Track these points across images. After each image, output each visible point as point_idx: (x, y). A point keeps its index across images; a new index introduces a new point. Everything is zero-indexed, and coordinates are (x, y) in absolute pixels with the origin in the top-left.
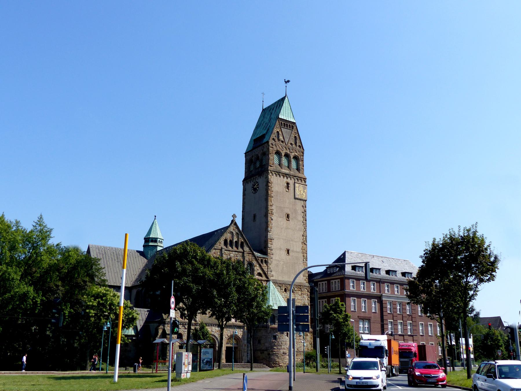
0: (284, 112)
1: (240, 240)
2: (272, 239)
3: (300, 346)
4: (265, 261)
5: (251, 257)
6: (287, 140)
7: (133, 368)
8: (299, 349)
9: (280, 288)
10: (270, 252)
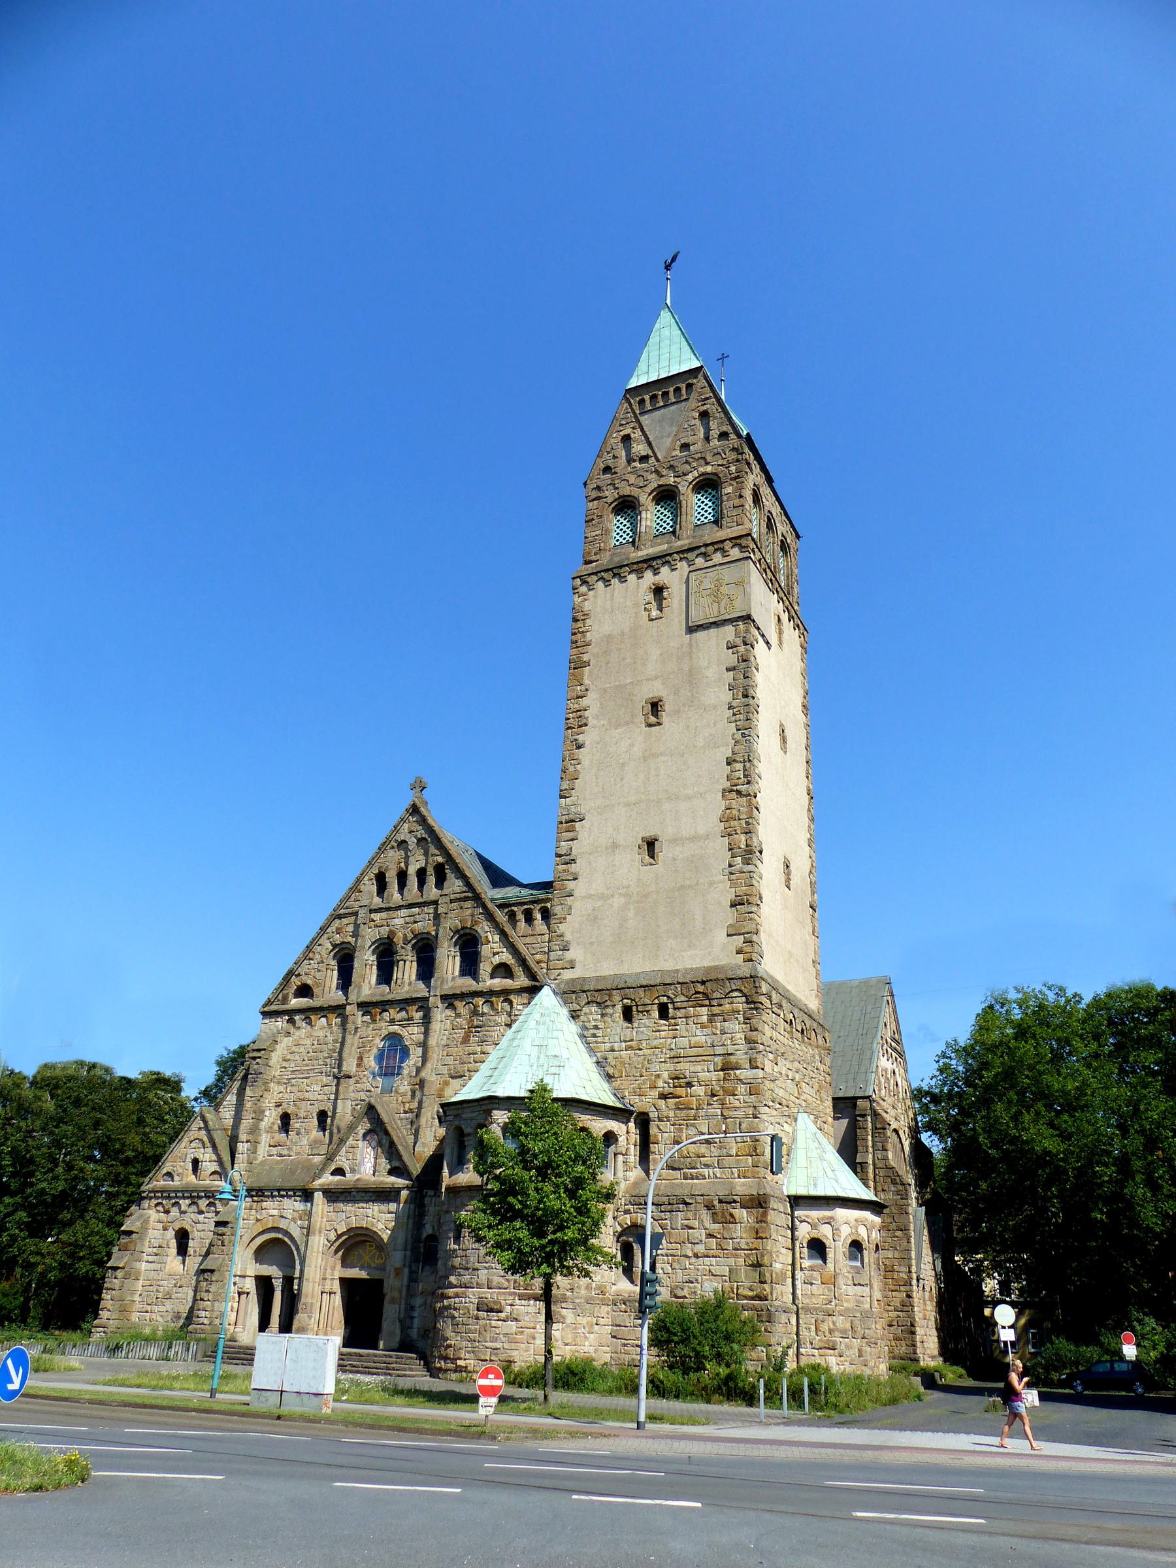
3: (686, 1278)
8: (679, 1293)
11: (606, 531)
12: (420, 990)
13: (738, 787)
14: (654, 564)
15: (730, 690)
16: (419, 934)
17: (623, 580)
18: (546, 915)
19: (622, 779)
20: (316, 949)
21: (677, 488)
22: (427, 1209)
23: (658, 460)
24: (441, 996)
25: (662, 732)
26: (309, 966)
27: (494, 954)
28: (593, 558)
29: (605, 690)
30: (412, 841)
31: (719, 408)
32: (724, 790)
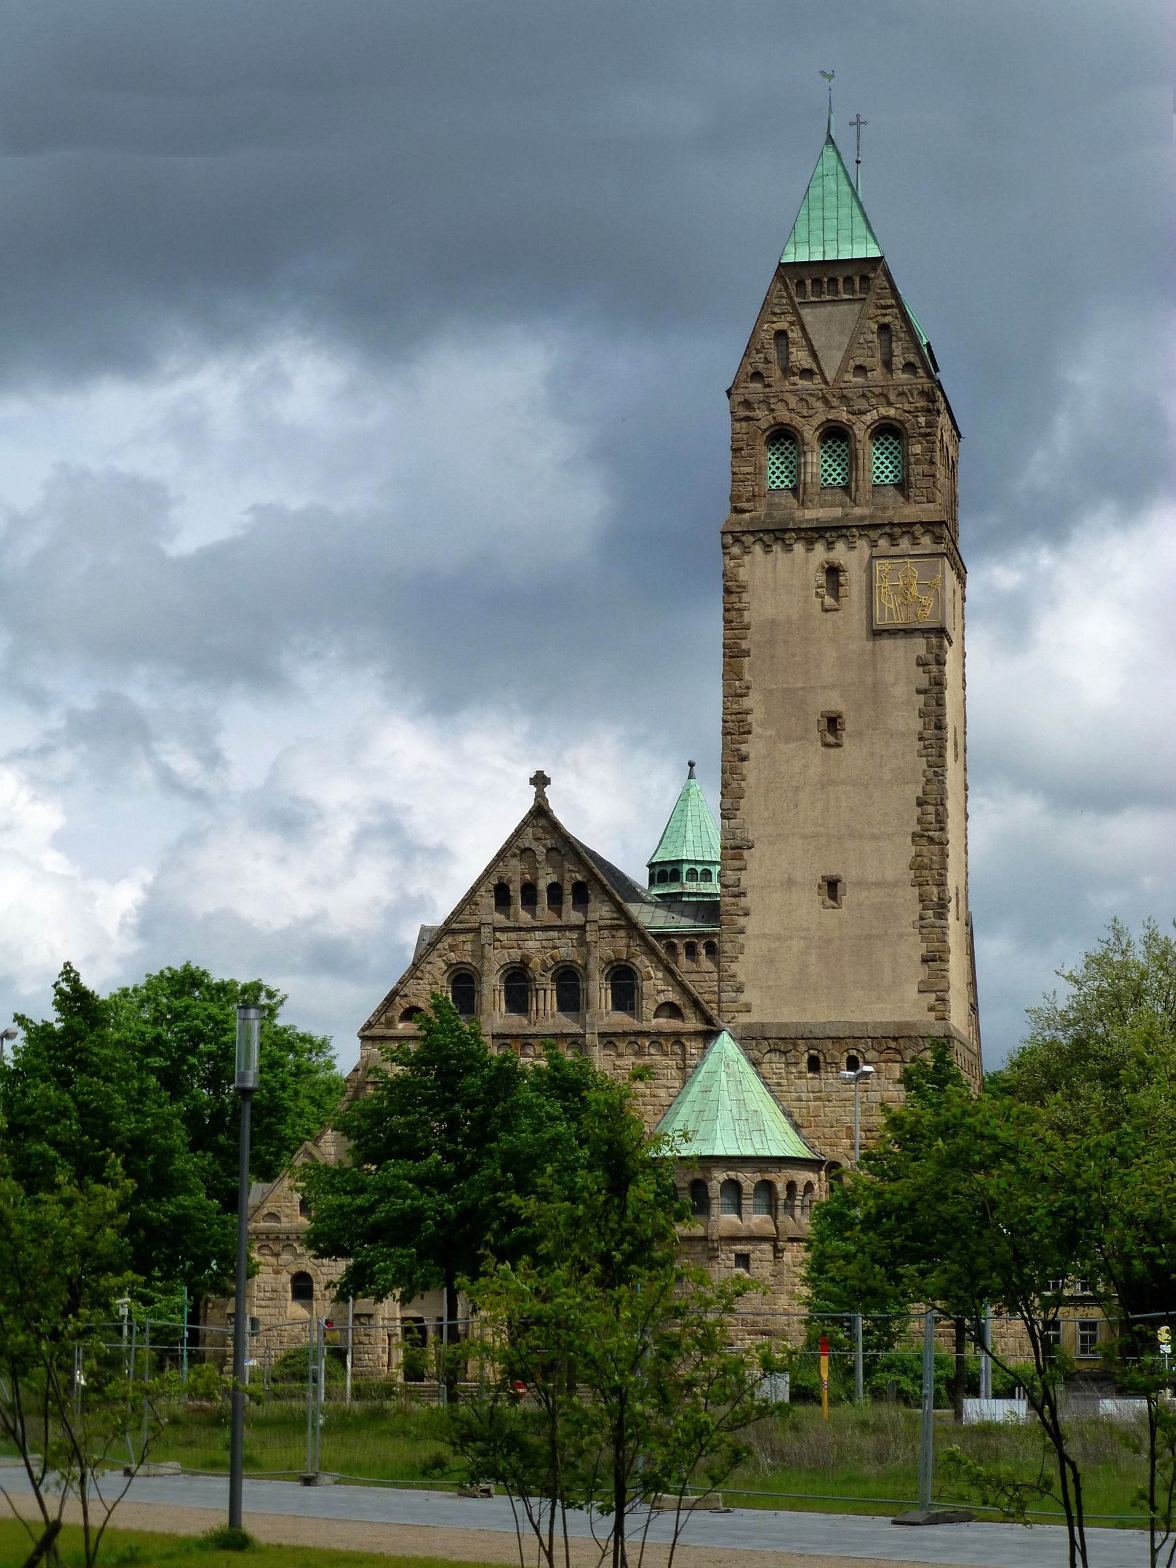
1: (567, 876)
2: (740, 848)
5: (624, 942)
6: (832, 363)
7: (964, 1400)
9: (783, 1060)
10: (733, 904)
11: (760, 468)
12: (565, 1023)
13: (931, 833)
14: (827, 535)
15: (921, 717)
16: (561, 961)
17: (788, 548)
18: (712, 950)
19: (796, 806)
20: (425, 967)
21: (852, 429)
23: (826, 382)
24: (599, 1034)
25: (842, 755)
26: (419, 987)
27: (659, 992)
28: (745, 505)
29: (771, 692)
30: (541, 852)
31: (903, 325)
32: (914, 834)
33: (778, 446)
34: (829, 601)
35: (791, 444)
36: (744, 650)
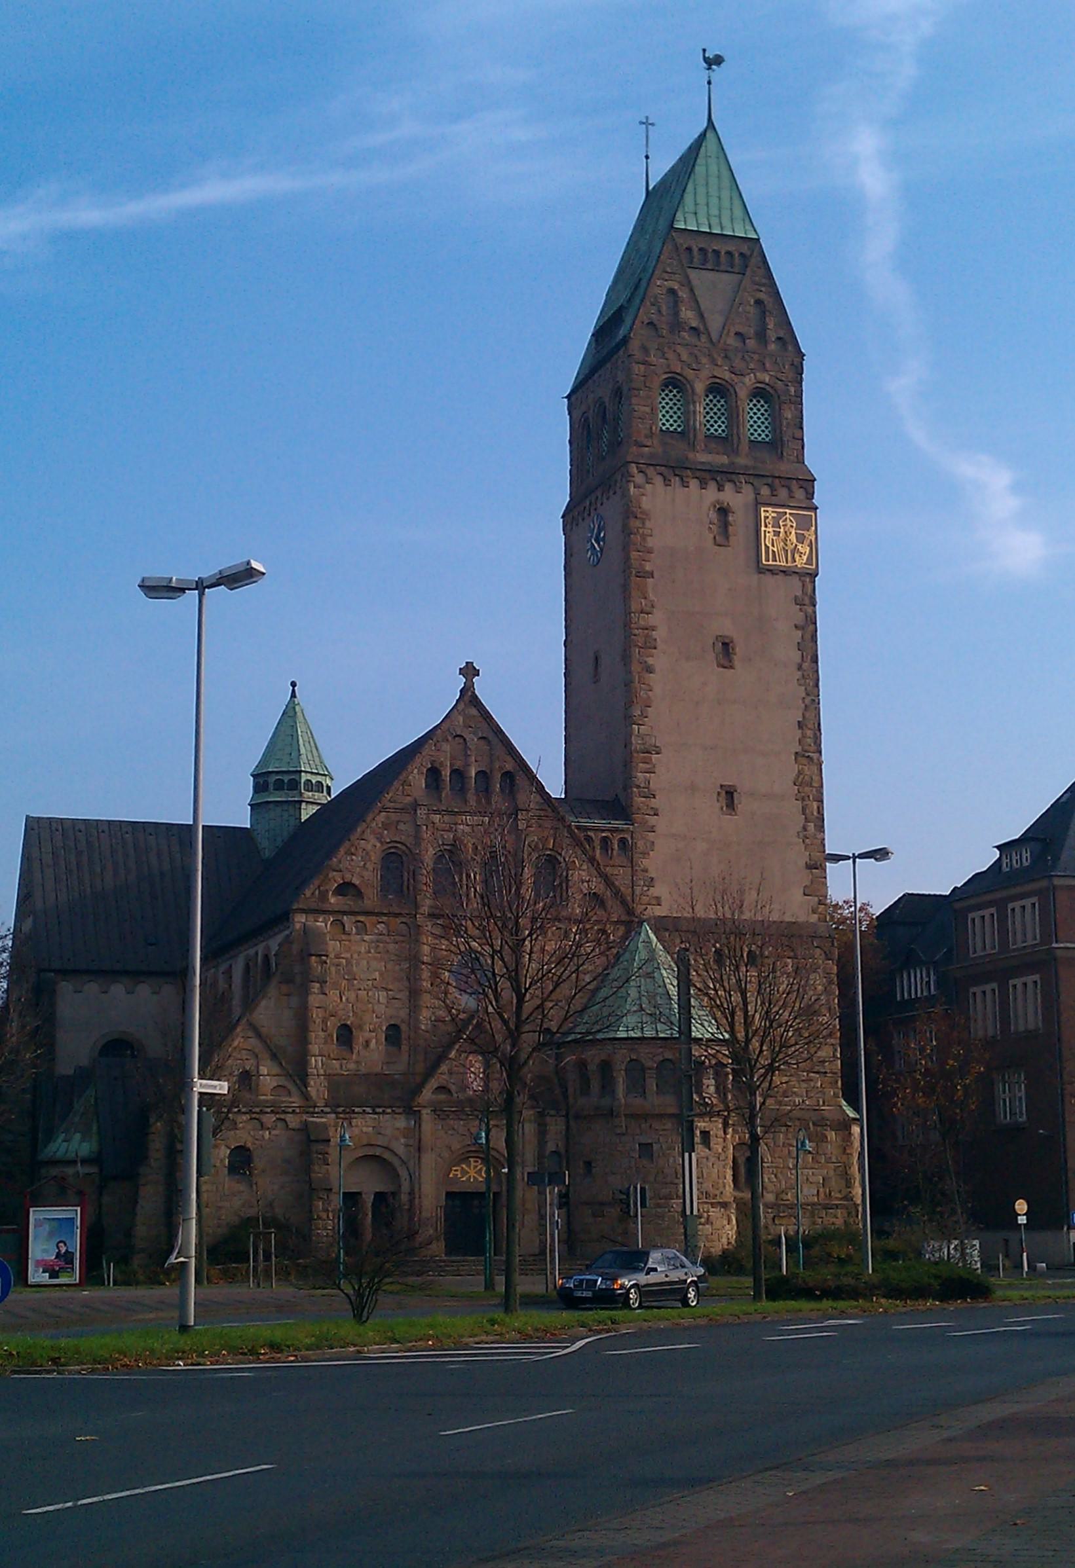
0: (701, 200)
4: (623, 841)
6: (715, 323)
22: (548, 1128)
32: (797, 753)
33: (667, 392)
34: (719, 539)
35: (678, 392)
36: (647, 572)
